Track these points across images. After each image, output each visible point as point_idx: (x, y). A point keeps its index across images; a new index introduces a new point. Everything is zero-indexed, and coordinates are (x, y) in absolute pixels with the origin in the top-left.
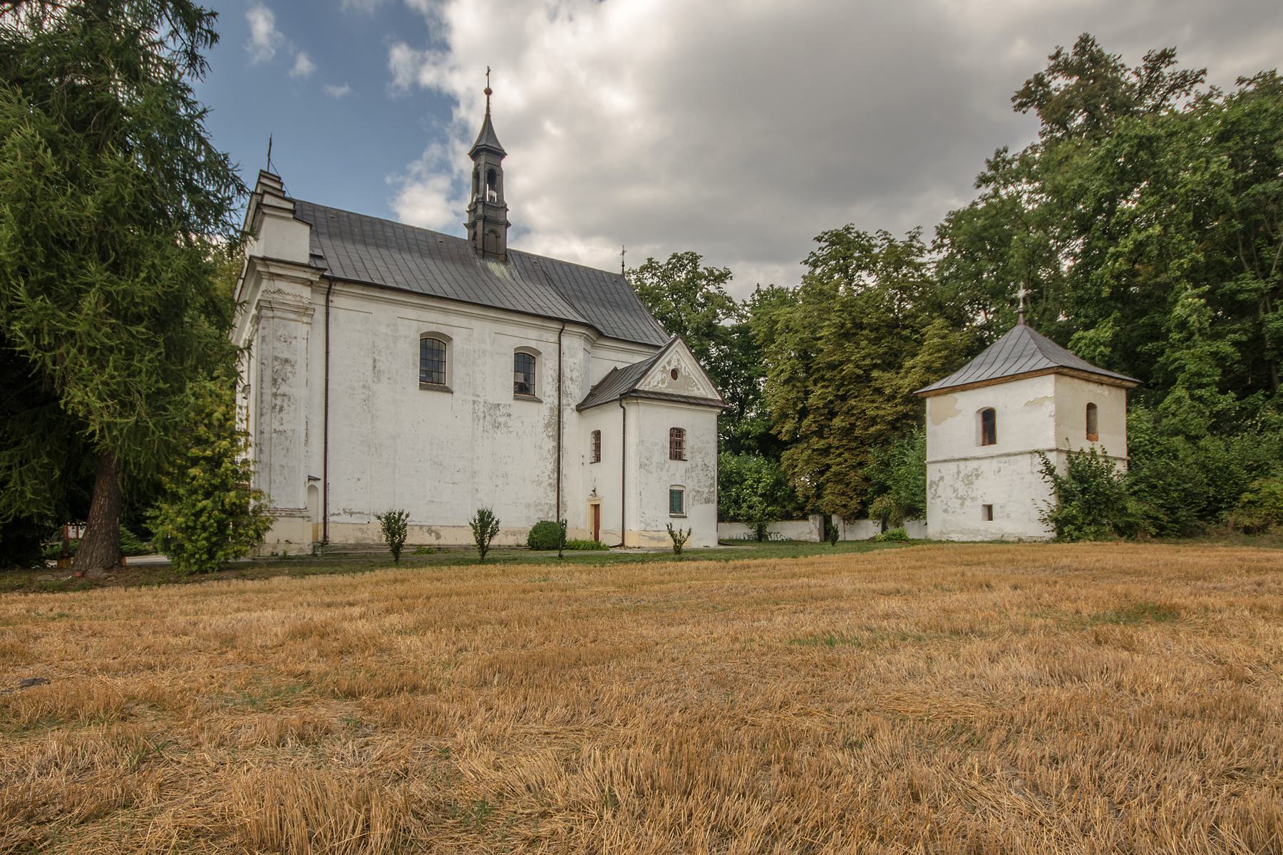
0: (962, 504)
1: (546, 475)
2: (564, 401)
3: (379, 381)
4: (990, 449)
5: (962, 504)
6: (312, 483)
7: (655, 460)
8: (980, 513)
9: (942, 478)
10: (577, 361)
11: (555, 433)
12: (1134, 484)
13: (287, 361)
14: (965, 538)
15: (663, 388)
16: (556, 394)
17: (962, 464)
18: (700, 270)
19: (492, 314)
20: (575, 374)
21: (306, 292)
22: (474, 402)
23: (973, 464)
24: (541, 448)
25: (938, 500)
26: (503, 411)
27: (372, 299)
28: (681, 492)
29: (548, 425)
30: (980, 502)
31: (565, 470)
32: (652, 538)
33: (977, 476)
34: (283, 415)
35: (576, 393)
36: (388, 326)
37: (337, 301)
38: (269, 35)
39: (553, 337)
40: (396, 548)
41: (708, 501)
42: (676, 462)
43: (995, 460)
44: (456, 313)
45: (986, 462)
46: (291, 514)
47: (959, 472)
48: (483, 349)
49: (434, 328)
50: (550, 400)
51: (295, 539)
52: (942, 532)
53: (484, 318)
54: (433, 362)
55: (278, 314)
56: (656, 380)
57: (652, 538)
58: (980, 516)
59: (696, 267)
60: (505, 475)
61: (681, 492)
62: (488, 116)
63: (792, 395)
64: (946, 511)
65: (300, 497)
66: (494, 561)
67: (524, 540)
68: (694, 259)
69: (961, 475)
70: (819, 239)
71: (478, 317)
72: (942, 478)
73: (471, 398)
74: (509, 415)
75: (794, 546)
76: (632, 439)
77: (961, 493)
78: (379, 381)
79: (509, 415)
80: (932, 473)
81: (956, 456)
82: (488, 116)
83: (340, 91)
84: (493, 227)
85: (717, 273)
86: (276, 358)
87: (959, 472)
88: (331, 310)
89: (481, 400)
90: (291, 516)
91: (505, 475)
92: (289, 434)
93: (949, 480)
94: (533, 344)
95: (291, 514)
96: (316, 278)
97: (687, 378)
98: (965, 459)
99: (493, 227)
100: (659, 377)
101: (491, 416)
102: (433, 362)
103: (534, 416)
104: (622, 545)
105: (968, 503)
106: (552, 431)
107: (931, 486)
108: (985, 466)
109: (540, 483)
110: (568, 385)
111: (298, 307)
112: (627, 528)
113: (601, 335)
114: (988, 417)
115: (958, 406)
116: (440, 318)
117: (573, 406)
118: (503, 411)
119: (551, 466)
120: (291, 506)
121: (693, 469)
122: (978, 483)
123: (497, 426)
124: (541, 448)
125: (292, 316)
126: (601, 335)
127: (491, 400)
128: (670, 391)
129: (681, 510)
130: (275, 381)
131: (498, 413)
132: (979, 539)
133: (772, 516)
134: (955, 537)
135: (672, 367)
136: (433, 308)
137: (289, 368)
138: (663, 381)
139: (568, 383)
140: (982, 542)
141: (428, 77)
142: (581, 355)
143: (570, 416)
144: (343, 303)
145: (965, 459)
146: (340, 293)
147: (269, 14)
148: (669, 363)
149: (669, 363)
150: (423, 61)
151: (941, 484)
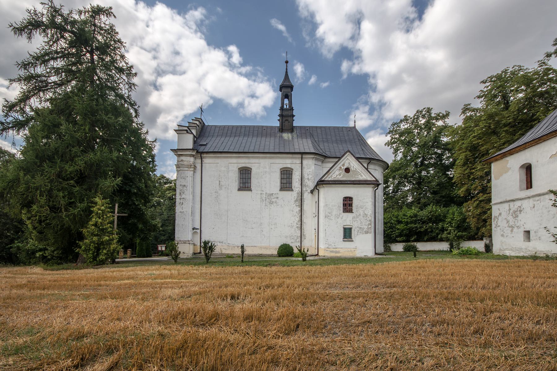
0: (512, 231)
1: (296, 222)
2: (304, 189)
3: (221, 189)
4: (530, 192)
5: (512, 231)
6: (195, 230)
7: (334, 213)
8: (521, 236)
9: (500, 214)
10: (311, 170)
11: (300, 204)
12: (411, 222)
13: (184, 186)
14: (513, 254)
15: (340, 178)
16: (300, 187)
17: (512, 204)
18: (433, 115)
19: (268, 155)
20: (310, 177)
21: (192, 159)
22: (261, 194)
23: (518, 203)
24: (293, 211)
25: (498, 228)
26: (275, 196)
27: (218, 157)
28: (351, 229)
29: (296, 201)
30: (522, 229)
31: (305, 220)
32: (332, 252)
33: (521, 211)
34: (183, 206)
35: (311, 184)
36: (225, 167)
37: (205, 161)
38: (302, 71)
39: (299, 161)
40: (208, 257)
41: (367, 232)
42: (347, 214)
43: (531, 199)
44: (253, 157)
45: (526, 201)
46: (185, 242)
47: (510, 209)
48: (267, 172)
49: (244, 165)
50: (297, 189)
51: (186, 251)
52: (500, 250)
53: (265, 158)
54: (245, 180)
55: (181, 169)
56: (337, 174)
57: (332, 252)
58: (522, 239)
59: (430, 115)
60: (276, 224)
61: (351, 229)
62: (287, 72)
63: (466, 172)
64: (502, 235)
65: (188, 236)
66: (214, 263)
67: (275, 252)
68: (429, 110)
69: (511, 211)
70: (484, 82)
71: (262, 158)
72: (500, 214)
73: (260, 192)
74: (277, 198)
75: (468, 254)
76: (322, 204)
77: (511, 223)
78: (221, 189)
79: (277, 198)
80: (495, 211)
81: (508, 199)
82: (287, 72)
83: (325, 85)
84: (287, 118)
85: (441, 115)
86: (181, 185)
87: (510, 209)
88: (203, 164)
89: (264, 193)
90: (185, 243)
91: (276, 224)
92: (185, 212)
93: (504, 215)
94: (289, 166)
95: (185, 242)
96: (194, 153)
97: (355, 171)
98: (513, 201)
99: (287, 118)
100: (337, 173)
101: (270, 199)
102: (245, 180)
103: (291, 197)
104: (318, 255)
105: (515, 230)
106: (298, 203)
107: (494, 220)
108: (526, 204)
109: (292, 227)
110: (306, 181)
111: (188, 165)
112: (320, 247)
113: (326, 157)
114: (528, 169)
115: (508, 166)
116: (246, 161)
117: (309, 191)
118: (275, 196)
119: (298, 219)
120: (186, 239)
121: (357, 217)
122: (521, 216)
123: (271, 203)
124: (293, 211)
125: (186, 169)
126: (326, 157)
127: (268, 192)
128: (344, 179)
129: (350, 237)
130: (180, 193)
131: (272, 197)
132: (521, 254)
133: (460, 238)
134: (508, 253)
135: (345, 167)
136: (242, 157)
137: (185, 188)
138: (340, 175)
139: (306, 181)
140: (517, 257)
141: (355, 69)
142: (313, 167)
143: (307, 196)
144: (208, 161)
145: (513, 201)
146: (205, 158)
147: (302, 65)
148: (343, 165)
149: (343, 165)
150: (354, 64)
151: (500, 218)
